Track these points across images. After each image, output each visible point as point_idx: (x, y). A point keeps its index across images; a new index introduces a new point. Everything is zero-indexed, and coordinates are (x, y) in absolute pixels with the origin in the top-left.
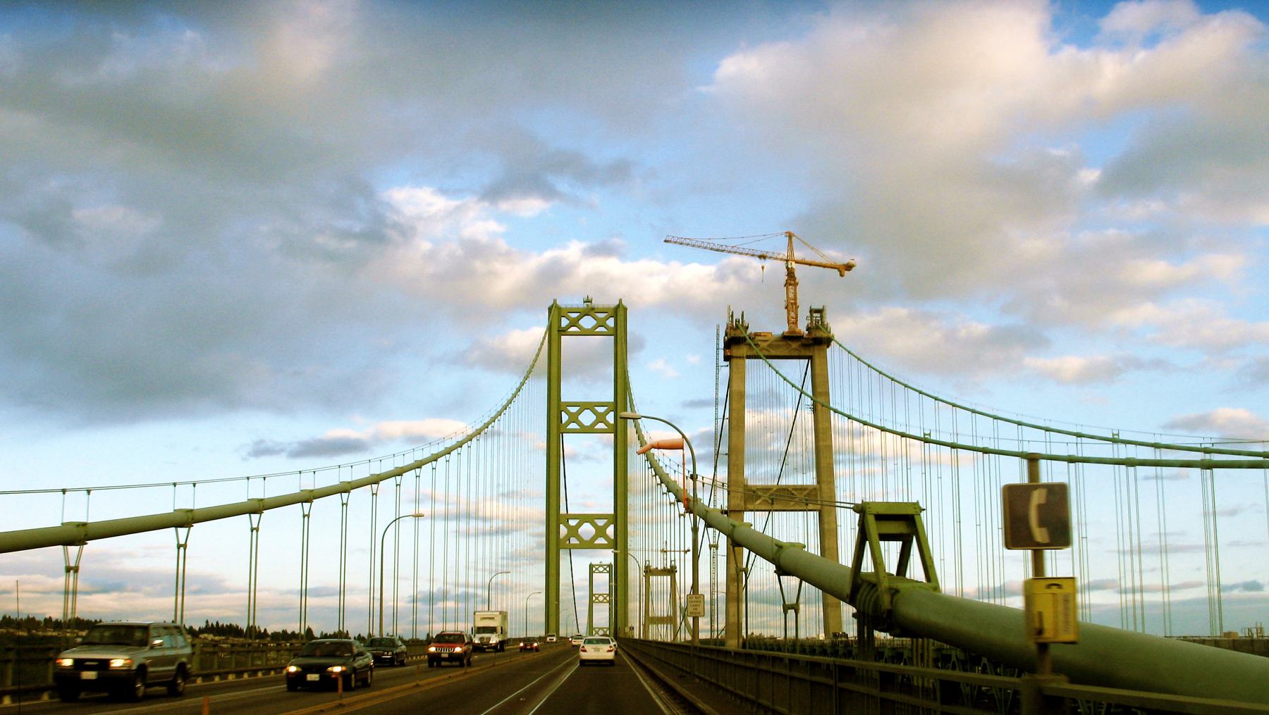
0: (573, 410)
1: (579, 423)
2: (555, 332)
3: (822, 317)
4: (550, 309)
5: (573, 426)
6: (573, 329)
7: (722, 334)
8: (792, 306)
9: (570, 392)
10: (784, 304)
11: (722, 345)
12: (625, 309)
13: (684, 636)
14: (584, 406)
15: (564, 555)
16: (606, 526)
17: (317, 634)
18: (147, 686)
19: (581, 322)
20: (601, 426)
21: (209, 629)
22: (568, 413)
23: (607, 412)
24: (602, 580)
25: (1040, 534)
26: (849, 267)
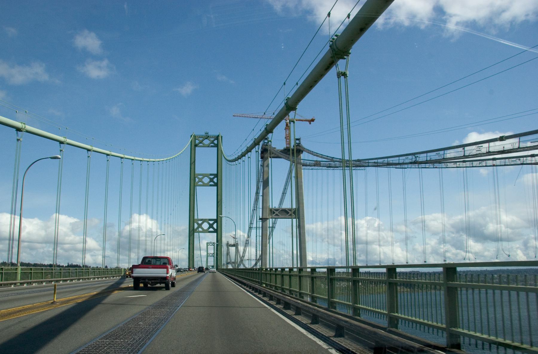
1: (203, 182)
2: (193, 146)
5: (200, 183)
8: (288, 138)
9: (199, 170)
10: (284, 136)
12: (222, 137)
14: (205, 175)
16: (214, 223)
17: (109, 268)
19: (204, 142)
20: (211, 229)
23: (214, 178)
24: (211, 251)
26: (313, 120)
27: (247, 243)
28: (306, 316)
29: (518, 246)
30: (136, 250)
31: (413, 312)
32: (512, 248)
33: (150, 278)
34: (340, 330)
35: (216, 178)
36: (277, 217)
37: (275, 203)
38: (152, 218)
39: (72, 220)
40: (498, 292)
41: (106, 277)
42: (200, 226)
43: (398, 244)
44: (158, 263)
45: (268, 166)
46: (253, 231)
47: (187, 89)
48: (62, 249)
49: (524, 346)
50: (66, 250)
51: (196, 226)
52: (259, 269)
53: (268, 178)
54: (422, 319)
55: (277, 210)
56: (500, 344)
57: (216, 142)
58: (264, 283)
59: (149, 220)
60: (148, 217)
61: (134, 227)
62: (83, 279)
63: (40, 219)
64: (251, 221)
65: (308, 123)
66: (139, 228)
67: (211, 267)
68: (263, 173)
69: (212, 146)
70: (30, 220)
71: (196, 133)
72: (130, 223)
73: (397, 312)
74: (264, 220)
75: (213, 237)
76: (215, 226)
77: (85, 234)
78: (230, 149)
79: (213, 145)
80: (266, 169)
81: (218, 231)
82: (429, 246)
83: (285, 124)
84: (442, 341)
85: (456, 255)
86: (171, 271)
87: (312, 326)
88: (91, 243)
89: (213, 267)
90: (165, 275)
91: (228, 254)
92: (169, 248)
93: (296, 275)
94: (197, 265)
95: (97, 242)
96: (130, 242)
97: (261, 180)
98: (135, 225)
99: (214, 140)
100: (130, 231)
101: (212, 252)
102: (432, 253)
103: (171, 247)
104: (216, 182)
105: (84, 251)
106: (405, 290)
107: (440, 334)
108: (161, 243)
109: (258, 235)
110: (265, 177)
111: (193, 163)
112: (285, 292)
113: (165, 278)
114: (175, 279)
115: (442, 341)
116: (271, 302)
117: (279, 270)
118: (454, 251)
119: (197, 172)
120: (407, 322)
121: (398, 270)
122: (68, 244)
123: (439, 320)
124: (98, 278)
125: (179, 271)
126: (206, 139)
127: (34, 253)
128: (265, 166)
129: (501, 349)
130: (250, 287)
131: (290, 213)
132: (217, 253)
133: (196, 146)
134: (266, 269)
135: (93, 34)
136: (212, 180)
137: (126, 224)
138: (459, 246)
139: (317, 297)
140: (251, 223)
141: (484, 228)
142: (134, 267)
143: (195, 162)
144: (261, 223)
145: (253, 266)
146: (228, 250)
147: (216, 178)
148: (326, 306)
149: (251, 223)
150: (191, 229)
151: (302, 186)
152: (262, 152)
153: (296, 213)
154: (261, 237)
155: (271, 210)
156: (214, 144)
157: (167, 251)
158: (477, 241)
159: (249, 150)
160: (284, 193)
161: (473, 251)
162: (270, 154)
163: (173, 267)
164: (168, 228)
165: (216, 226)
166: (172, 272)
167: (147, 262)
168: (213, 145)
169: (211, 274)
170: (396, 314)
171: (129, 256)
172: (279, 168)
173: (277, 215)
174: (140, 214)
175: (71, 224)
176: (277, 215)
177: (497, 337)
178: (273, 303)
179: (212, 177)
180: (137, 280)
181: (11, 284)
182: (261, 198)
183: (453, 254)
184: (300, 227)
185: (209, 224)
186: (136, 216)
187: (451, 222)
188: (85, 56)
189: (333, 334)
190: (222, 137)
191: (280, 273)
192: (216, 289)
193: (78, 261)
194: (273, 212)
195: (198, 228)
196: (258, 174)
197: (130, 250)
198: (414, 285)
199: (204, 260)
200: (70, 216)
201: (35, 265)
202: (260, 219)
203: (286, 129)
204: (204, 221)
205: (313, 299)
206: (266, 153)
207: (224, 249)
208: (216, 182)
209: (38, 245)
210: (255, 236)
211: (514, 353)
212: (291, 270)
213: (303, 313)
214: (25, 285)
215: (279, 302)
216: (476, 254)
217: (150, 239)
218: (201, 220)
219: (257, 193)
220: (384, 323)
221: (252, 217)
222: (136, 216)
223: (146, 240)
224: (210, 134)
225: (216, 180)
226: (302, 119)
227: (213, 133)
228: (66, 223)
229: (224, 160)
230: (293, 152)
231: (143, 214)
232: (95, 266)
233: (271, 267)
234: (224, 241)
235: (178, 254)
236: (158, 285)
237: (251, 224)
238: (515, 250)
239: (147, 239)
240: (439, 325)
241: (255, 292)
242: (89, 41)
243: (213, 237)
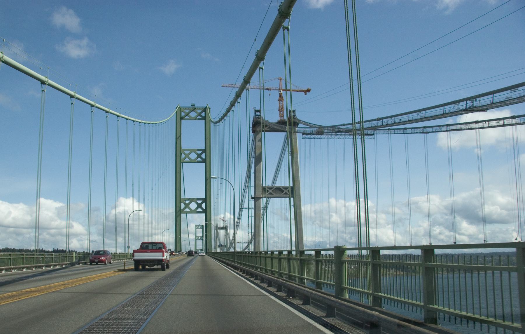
1: (190, 159)
5: (187, 160)
6: (187, 117)
7: (251, 121)
8: (281, 110)
9: (185, 145)
10: (278, 107)
11: (251, 126)
12: (210, 109)
13: (232, 250)
14: (191, 151)
15: (183, 216)
16: (202, 203)
19: (190, 114)
21: (55, 251)
22: (185, 154)
23: (202, 154)
26: (308, 91)
27: (236, 226)
28: (275, 287)
29: (513, 228)
30: (123, 234)
31: (464, 303)
32: (507, 230)
33: (147, 260)
34: (331, 310)
35: (204, 154)
36: (271, 195)
38: (139, 201)
39: (58, 205)
40: (497, 273)
42: (187, 206)
43: (390, 226)
44: (154, 248)
45: (260, 140)
46: (245, 213)
47: (171, 68)
48: (49, 234)
49: (490, 319)
50: (53, 235)
51: (183, 206)
52: (252, 252)
53: (261, 154)
54: (403, 298)
55: (271, 188)
56: (468, 319)
60: (135, 201)
61: (121, 211)
62: (36, 267)
63: (25, 203)
64: (242, 201)
65: (303, 93)
66: (125, 212)
67: (200, 251)
68: (255, 148)
69: (199, 119)
70: (15, 205)
72: (116, 207)
73: (381, 292)
74: (256, 199)
75: (201, 219)
76: (204, 206)
77: (68, 218)
79: (200, 117)
80: (258, 143)
81: (207, 212)
82: (421, 228)
83: (279, 95)
84: (419, 316)
85: (450, 237)
86: (166, 254)
87: (261, 284)
88: (78, 228)
89: (202, 250)
90: (161, 258)
91: (217, 236)
92: (157, 231)
94: (185, 248)
95: (83, 226)
96: (116, 228)
97: (253, 155)
98: (121, 209)
99: (201, 113)
100: (116, 215)
101: (201, 235)
102: (424, 235)
103: (159, 231)
105: (68, 236)
106: (402, 273)
107: (399, 306)
108: (148, 227)
109: (250, 215)
110: (258, 152)
111: (178, 138)
112: (274, 274)
113: (162, 261)
114: (169, 261)
115: (419, 316)
116: (270, 289)
117: (269, 253)
118: (447, 233)
119: (184, 147)
120: (389, 301)
121: (437, 251)
122: (54, 229)
123: (470, 306)
125: (171, 254)
126: (193, 111)
127: (20, 238)
128: (257, 140)
129: (478, 325)
130: (244, 271)
131: (285, 191)
132: (206, 235)
133: (182, 118)
134: (261, 252)
135: (71, 12)
136: (199, 156)
137: (112, 208)
138: (454, 228)
139: (321, 283)
140: (242, 204)
141: (478, 210)
142: (135, 251)
143: (180, 136)
144: (253, 203)
145: (245, 249)
146: (217, 232)
147: (204, 154)
148: (370, 304)
149: (242, 204)
150: (178, 209)
152: (254, 126)
153: (291, 192)
154: (253, 218)
155: (264, 188)
156: (201, 116)
157: (155, 234)
158: (471, 223)
160: (277, 171)
161: (466, 233)
162: (263, 127)
163: (167, 252)
164: (155, 211)
165: (205, 206)
166: (167, 255)
167: (145, 247)
168: (200, 117)
169: (200, 257)
170: (380, 294)
171: (116, 240)
173: (271, 193)
174: (126, 198)
175: (56, 208)
176: (271, 193)
177: (461, 310)
178: (264, 285)
179: (199, 152)
180: (137, 263)
181: (33, 267)
182: (252, 176)
183: (446, 236)
184: (297, 207)
185: (197, 203)
186: (122, 200)
187: (445, 203)
188: (64, 34)
189: (276, 290)
190: (210, 109)
191: (270, 256)
192: (208, 275)
193: (62, 246)
194: (265, 190)
195: (185, 208)
196: (250, 149)
197: (116, 233)
198: (434, 268)
199: (193, 243)
200: (55, 200)
201: (20, 250)
202: (252, 198)
203: (279, 100)
204: (192, 200)
205: (319, 285)
207: (213, 231)
209: (24, 231)
210: (247, 219)
211: (505, 332)
212: (290, 252)
213: (312, 303)
214: (44, 268)
215: (280, 288)
216: (470, 236)
217: (137, 223)
218: (189, 199)
219: (249, 171)
220: (368, 302)
221: (243, 196)
222: (122, 200)
224: (196, 106)
225: (204, 156)
226: (296, 89)
227: (200, 104)
228: (50, 208)
230: (288, 125)
231: (129, 198)
232: (82, 251)
233: (266, 250)
234: (213, 223)
235: (168, 238)
236: (155, 267)
237: (242, 204)
238: (511, 232)
239: (134, 222)
240: (418, 303)
242: (67, 19)
243: (201, 219)
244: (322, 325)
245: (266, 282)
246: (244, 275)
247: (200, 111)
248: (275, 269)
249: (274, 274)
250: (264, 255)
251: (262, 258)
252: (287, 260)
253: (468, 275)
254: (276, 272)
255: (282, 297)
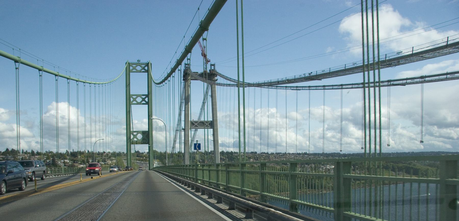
0: (134, 97)
1: (136, 101)
3: (214, 67)
4: (126, 63)
5: (135, 102)
11: (182, 76)
12: (151, 64)
14: (138, 96)
18: (35, 178)
22: (133, 98)
23: (145, 98)
25: (197, 149)
28: (226, 204)
37: (194, 117)
41: (55, 175)
55: (196, 122)
57: (146, 68)
58: (200, 180)
59: (73, 110)
69: (143, 72)
71: (130, 61)
78: (158, 74)
79: (143, 70)
87: (218, 205)
93: (201, 169)
97: (184, 98)
99: (145, 67)
104: (147, 101)
111: (128, 85)
124: (58, 175)
147: (147, 98)
151: (216, 102)
152: (184, 76)
159: (173, 70)
162: (192, 77)
168: (143, 70)
170: (265, 193)
172: (198, 88)
174: (57, 102)
189: (216, 202)
194: (193, 123)
206: (187, 76)
208: (147, 101)
223: (85, 142)
225: (147, 100)
227: (144, 60)
229: (153, 84)
230: (210, 76)
241: (196, 191)
244: (217, 210)
245: (207, 194)
246: (183, 186)
247: (144, 66)
248: (206, 179)
249: (205, 183)
250: (201, 168)
251: (205, 171)
252: (240, 175)
253: (393, 186)
254: (207, 181)
255: (213, 204)
